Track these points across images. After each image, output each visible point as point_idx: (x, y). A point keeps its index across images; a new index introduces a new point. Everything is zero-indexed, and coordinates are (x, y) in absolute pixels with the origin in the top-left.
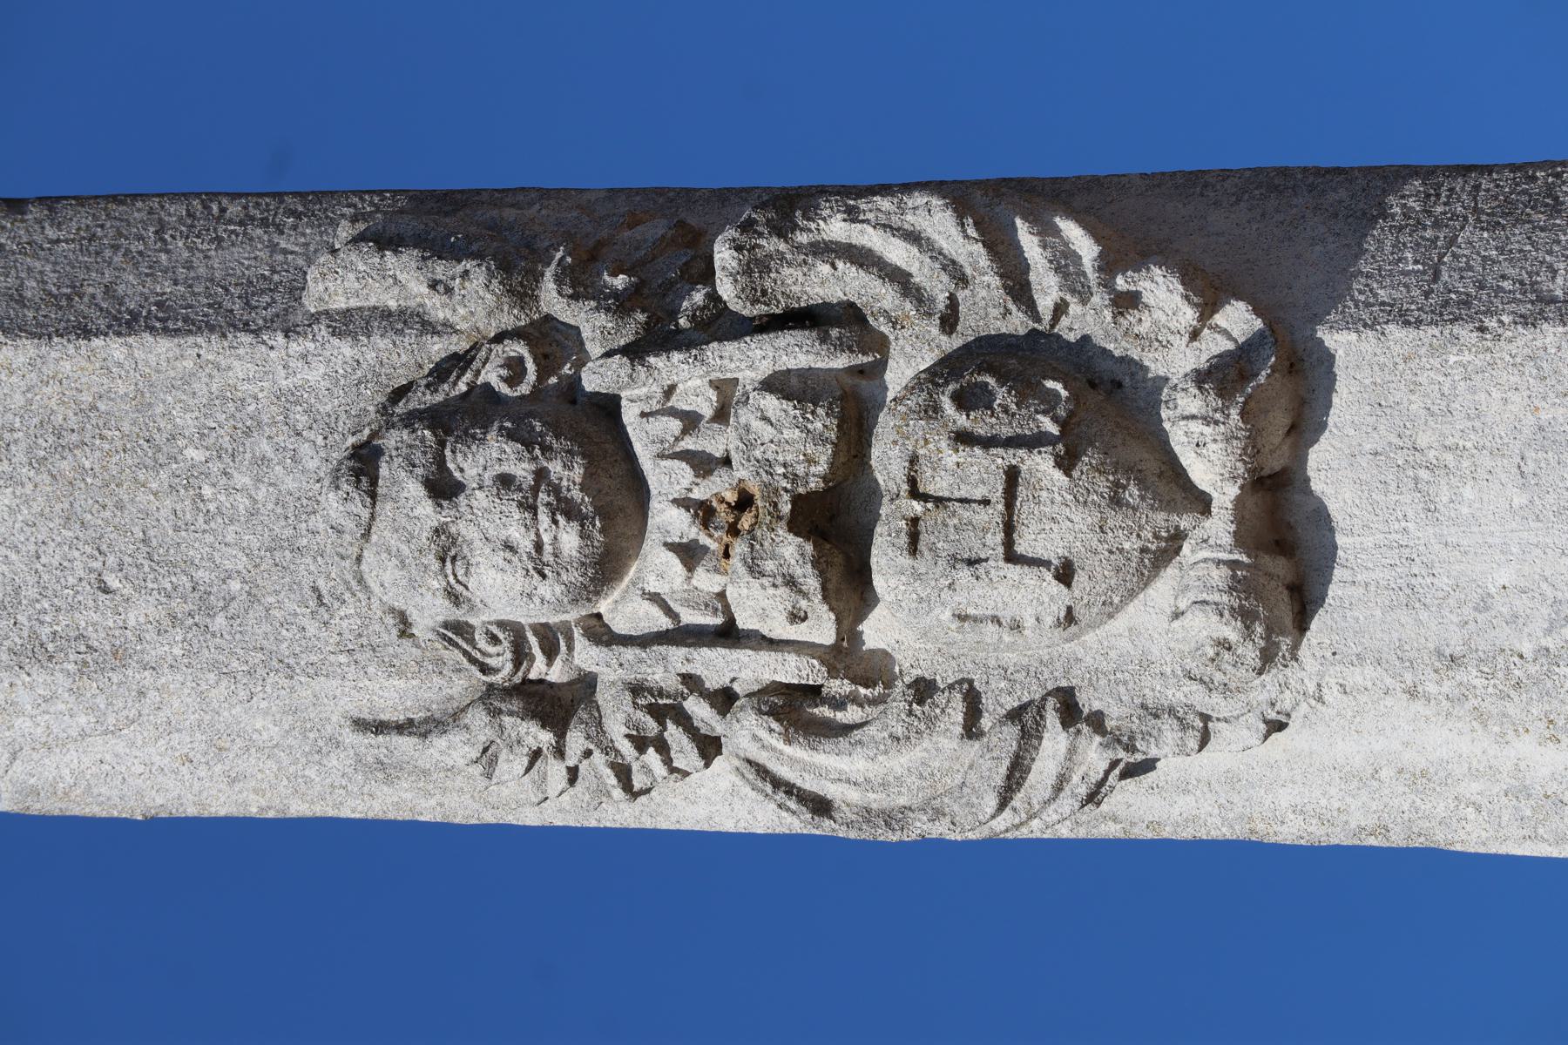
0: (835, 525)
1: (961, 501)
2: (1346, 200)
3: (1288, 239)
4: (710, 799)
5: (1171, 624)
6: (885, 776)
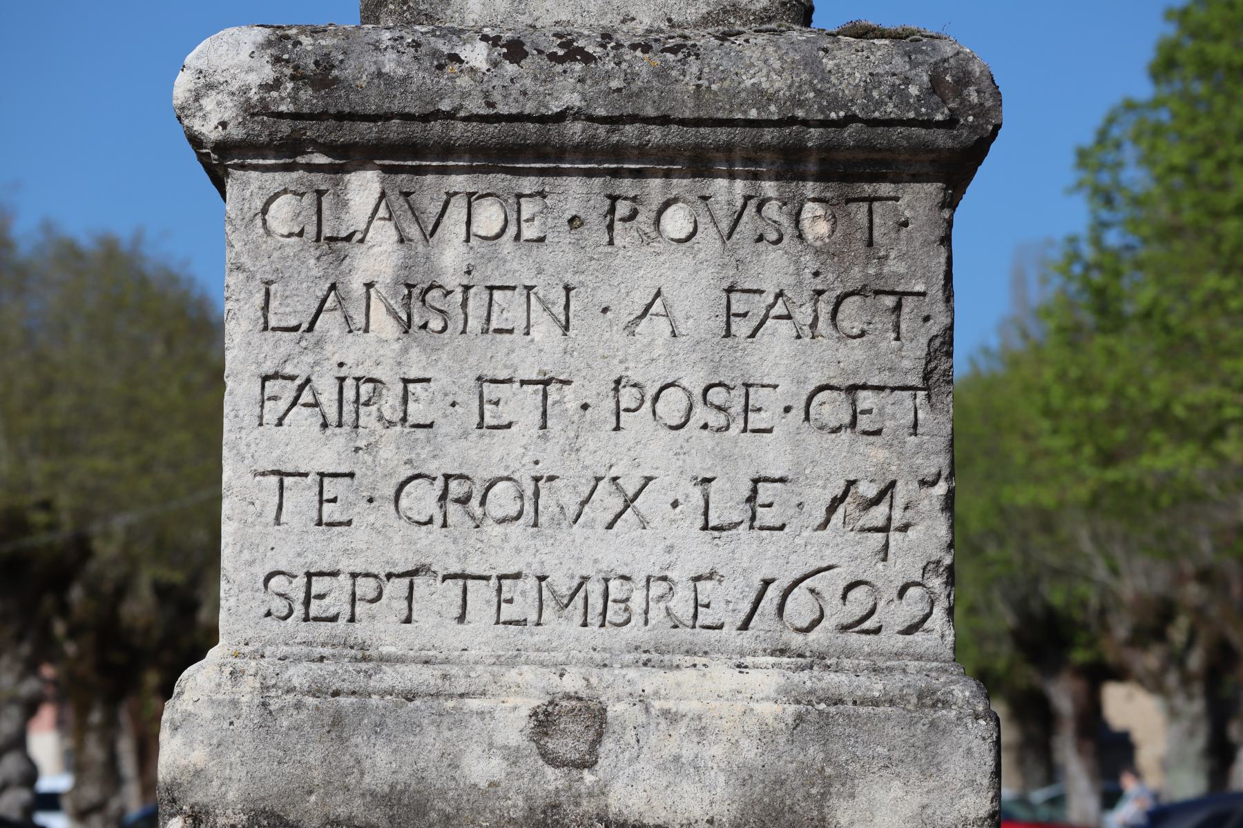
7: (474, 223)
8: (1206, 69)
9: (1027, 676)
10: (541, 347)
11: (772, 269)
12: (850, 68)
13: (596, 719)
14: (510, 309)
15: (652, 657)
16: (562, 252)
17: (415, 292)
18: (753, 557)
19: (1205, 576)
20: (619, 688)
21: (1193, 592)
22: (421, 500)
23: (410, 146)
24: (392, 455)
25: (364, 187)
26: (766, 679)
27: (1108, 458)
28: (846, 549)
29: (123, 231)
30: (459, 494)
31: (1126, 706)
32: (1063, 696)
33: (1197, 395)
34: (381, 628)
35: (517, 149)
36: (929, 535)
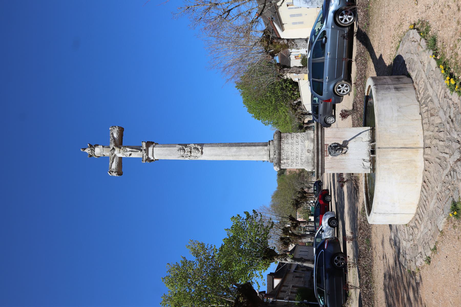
0: (191, 152)
1: (399, 46)
2: (203, 144)
3: (202, 145)
4: (187, 159)
5: (199, 154)
6: (192, 158)
7: (283, 156)
8: (259, 116)
9: (304, 129)
10: (290, 153)
11: (286, 142)
12: (276, 138)
13: (308, 150)
14: (288, 154)
15: (305, 147)
16: (285, 152)
17: (287, 159)
18: (300, 142)
19: (296, 116)
20: (307, 149)
21: (297, 116)
22: (297, 159)
23: (280, 160)
24: (295, 160)
25: (282, 162)
26: (306, 141)
27: (288, 123)
28: (299, 138)
29: (271, 197)
30: (297, 157)
31: (306, 121)
32: (305, 126)
33: (283, 117)
34: (304, 161)
35: (280, 154)
36: (299, 134)
